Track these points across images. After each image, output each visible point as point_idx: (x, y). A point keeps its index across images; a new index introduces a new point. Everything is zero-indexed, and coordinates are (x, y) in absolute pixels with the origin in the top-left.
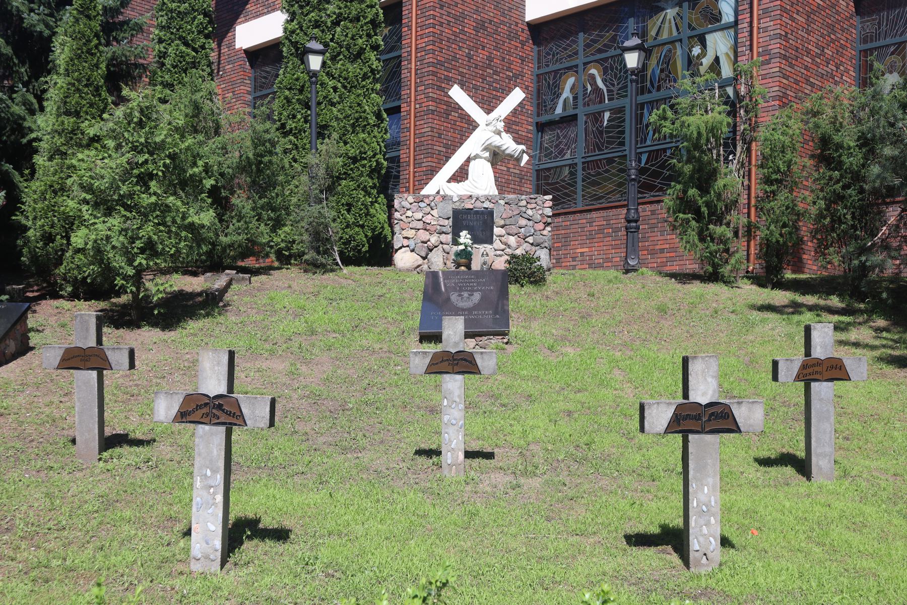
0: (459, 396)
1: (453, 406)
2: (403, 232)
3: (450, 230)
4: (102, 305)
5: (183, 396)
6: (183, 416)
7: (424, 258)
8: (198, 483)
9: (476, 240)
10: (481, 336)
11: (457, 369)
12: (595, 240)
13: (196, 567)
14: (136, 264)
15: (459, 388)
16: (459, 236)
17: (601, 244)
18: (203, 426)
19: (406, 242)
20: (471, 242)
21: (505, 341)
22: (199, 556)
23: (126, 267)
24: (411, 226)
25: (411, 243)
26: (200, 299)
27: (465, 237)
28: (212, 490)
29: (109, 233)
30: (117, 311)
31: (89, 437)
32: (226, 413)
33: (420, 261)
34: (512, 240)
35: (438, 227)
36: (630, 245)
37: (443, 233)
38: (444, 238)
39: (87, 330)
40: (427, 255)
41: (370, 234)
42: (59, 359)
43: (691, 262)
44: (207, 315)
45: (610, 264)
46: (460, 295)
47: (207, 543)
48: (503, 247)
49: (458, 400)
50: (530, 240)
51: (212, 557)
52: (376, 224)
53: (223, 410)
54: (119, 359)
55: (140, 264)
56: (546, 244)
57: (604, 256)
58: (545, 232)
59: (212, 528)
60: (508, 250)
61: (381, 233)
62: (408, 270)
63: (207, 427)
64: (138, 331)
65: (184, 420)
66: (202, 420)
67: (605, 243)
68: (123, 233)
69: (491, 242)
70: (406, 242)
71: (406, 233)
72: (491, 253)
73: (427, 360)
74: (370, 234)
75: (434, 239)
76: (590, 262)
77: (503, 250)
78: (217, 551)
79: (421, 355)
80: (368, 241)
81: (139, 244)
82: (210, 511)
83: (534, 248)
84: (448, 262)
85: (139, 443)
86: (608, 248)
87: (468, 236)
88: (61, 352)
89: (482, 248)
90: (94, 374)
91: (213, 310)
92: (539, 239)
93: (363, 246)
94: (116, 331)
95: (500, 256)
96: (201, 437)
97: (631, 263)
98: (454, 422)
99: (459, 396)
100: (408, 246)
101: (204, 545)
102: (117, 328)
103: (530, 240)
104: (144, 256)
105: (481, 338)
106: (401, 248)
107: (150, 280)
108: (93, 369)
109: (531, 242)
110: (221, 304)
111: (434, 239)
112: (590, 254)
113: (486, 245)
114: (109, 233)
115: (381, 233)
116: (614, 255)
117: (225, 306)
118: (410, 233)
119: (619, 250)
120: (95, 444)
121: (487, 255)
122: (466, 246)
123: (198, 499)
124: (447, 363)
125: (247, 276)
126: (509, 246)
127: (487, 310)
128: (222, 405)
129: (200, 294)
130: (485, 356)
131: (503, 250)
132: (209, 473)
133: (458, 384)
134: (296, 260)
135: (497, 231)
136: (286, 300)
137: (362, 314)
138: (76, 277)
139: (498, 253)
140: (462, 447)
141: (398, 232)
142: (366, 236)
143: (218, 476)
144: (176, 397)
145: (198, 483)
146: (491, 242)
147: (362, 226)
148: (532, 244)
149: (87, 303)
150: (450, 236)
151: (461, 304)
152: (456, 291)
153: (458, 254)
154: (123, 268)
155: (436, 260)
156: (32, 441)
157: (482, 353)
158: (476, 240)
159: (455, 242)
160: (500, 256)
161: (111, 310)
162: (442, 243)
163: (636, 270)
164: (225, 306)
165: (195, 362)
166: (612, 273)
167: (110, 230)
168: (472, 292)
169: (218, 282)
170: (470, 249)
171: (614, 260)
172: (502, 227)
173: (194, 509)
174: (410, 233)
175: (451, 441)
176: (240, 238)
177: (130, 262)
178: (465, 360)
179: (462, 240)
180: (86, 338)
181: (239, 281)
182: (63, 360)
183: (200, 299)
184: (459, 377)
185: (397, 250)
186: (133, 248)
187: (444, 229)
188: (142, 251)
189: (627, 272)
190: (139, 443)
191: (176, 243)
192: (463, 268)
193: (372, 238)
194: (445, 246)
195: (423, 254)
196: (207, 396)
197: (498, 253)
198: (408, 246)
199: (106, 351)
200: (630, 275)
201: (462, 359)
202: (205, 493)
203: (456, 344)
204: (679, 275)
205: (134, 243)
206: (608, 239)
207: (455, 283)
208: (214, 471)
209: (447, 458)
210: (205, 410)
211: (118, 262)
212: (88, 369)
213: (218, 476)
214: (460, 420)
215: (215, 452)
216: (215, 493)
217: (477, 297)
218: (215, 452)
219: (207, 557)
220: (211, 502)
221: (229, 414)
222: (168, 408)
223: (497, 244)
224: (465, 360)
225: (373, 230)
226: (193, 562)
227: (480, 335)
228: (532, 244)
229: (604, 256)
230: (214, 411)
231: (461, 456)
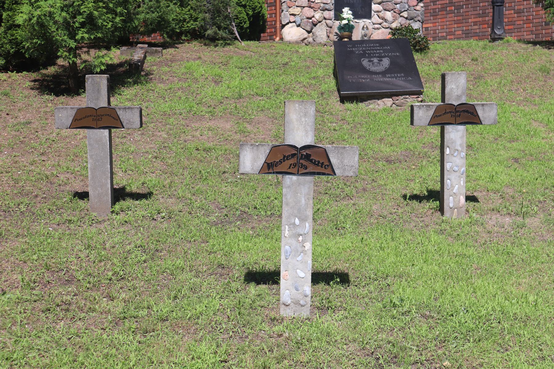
0: (461, 145)
1: (456, 154)
2: (290, 10)
3: (333, 7)
4: (34, 75)
5: (270, 148)
6: (269, 167)
7: (309, 32)
8: (287, 232)
9: (357, 16)
10: (397, 96)
11: (459, 120)
12: (438, 17)
13: (285, 312)
14: (78, 37)
15: (462, 137)
16: (342, 12)
17: (445, 20)
18: (290, 176)
19: (292, 19)
20: (353, 17)
21: (420, 99)
22: (289, 302)
23: (68, 40)
24: (297, 4)
25: (298, 19)
26: (122, 69)
27: (347, 13)
28: (301, 238)
29: (52, 9)
30: (51, 81)
31: (100, 192)
32: (314, 163)
33: (306, 35)
34: (389, 15)
35: (322, 5)
36: (496, 17)
37: (326, 9)
38: (326, 14)
39: (99, 91)
40: (312, 29)
41: (251, 13)
42: (71, 119)
43: (528, 33)
44: (135, 83)
45: (452, 37)
46: (370, 61)
47: (297, 290)
48: (380, 21)
49: (460, 149)
50: (405, 14)
51: (302, 302)
52: (257, 4)
53: (311, 161)
54: (129, 118)
55: (83, 38)
56: (419, 18)
57: (448, 30)
58: (418, 8)
59: (302, 274)
60: (385, 24)
61: (259, 12)
62: (297, 43)
63: (294, 178)
64: (79, 98)
65: (271, 171)
66: (289, 171)
67: (448, 19)
68: (65, 9)
69: (369, 17)
70: (292, 19)
71: (292, 11)
72: (370, 27)
73: (431, 113)
74: (251, 13)
75: (318, 15)
76: (434, 35)
77: (380, 24)
78: (306, 296)
79: (424, 109)
80: (249, 19)
81: (80, 19)
82: (299, 258)
83: (408, 22)
84: (331, 35)
85: (137, 196)
86: (450, 23)
87: (350, 12)
88: (74, 112)
89: (362, 22)
90: (106, 132)
91: (138, 78)
92: (413, 13)
93: (245, 23)
94: (57, 98)
95: (378, 29)
96: (289, 187)
97: (497, 32)
98: (456, 169)
99: (461, 145)
100: (294, 22)
101: (294, 291)
102: (57, 95)
103: (405, 14)
104: (85, 30)
105: (397, 98)
106: (288, 24)
107: (85, 52)
108: (104, 128)
109: (406, 16)
110: (143, 73)
111: (318, 15)
112: (434, 28)
113: (365, 20)
114: (52, 9)
115: (259, 12)
116: (457, 29)
117: (147, 75)
118: (297, 11)
119: (461, 25)
120: (108, 198)
121: (367, 28)
122: (349, 21)
123: (287, 247)
124: (449, 115)
125: (160, 49)
126: (386, 21)
127: (400, 73)
128: (310, 155)
129: (121, 65)
130: (486, 108)
131: (380, 24)
132: (297, 221)
133: (460, 134)
134: (186, 36)
135: (375, 7)
136: (200, 70)
137: (278, 80)
138: (9, 51)
139: (377, 26)
140: (464, 191)
141: (285, 10)
142: (248, 14)
143: (307, 225)
144: (262, 149)
145: (287, 232)
146: (369, 17)
147: (244, 6)
148: (406, 18)
149: (20, 74)
150: (332, 13)
151: (373, 69)
152: (365, 57)
153: (341, 28)
154: (65, 41)
155: (320, 33)
156: (36, 196)
157: (483, 105)
158: (357, 16)
159: (338, 17)
160: (378, 29)
161: (44, 80)
162: (325, 19)
163: (502, 39)
164: (147, 75)
165: (284, 116)
166: (486, 42)
167: (52, 6)
168: (380, 58)
169: (137, 54)
170: (352, 23)
171: (457, 33)
172: (379, 4)
173: (283, 257)
174: (297, 11)
175: (453, 187)
176: (154, 15)
177: (72, 36)
178: (467, 112)
179: (345, 15)
180: (97, 99)
181: (152, 53)
182: (75, 120)
183: (122, 69)
184: (461, 128)
185: (283, 26)
186: (74, 23)
187: (327, 7)
188: (83, 25)
189: (494, 40)
190: (137, 196)
191: (113, 18)
192: (346, 40)
193: (252, 16)
194: (328, 21)
195: (308, 29)
196: (294, 147)
197: (377, 26)
198: (294, 22)
199: (117, 110)
200: (497, 43)
201: (464, 111)
202: (293, 242)
203: (459, 97)
204: (543, 42)
205: (76, 18)
206: (450, 15)
207: (363, 51)
208: (303, 220)
209: (449, 201)
210: (292, 161)
211: (61, 36)
212: (100, 128)
213: (307, 225)
214: (462, 167)
215: (303, 201)
216: (303, 241)
217: (386, 62)
218: (303, 201)
219: (297, 303)
220: (300, 249)
221: (317, 163)
222: (254, 160)
223: (375, 18)
224: (467, 112)
225: (254, 9)
226: (282, 307)
227: (397, 94)
228: (406, 18)
229: (448, 30)
230: (301, 161)
231: (463, 199)
